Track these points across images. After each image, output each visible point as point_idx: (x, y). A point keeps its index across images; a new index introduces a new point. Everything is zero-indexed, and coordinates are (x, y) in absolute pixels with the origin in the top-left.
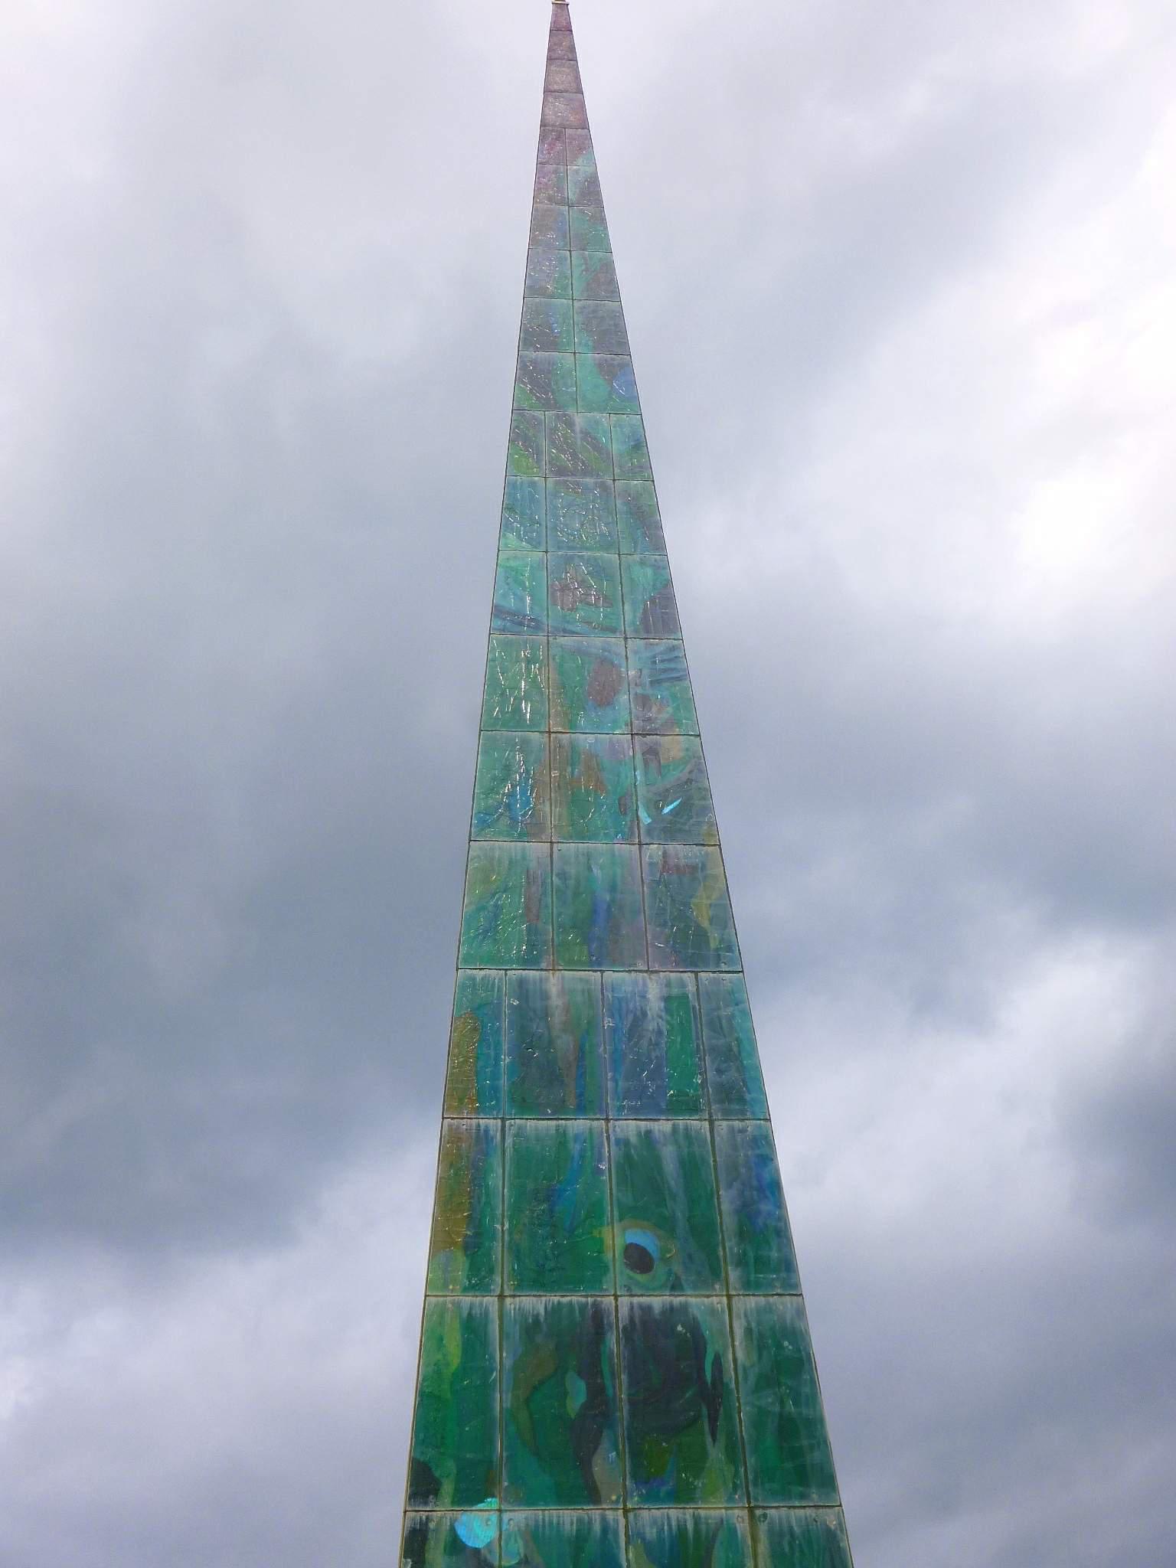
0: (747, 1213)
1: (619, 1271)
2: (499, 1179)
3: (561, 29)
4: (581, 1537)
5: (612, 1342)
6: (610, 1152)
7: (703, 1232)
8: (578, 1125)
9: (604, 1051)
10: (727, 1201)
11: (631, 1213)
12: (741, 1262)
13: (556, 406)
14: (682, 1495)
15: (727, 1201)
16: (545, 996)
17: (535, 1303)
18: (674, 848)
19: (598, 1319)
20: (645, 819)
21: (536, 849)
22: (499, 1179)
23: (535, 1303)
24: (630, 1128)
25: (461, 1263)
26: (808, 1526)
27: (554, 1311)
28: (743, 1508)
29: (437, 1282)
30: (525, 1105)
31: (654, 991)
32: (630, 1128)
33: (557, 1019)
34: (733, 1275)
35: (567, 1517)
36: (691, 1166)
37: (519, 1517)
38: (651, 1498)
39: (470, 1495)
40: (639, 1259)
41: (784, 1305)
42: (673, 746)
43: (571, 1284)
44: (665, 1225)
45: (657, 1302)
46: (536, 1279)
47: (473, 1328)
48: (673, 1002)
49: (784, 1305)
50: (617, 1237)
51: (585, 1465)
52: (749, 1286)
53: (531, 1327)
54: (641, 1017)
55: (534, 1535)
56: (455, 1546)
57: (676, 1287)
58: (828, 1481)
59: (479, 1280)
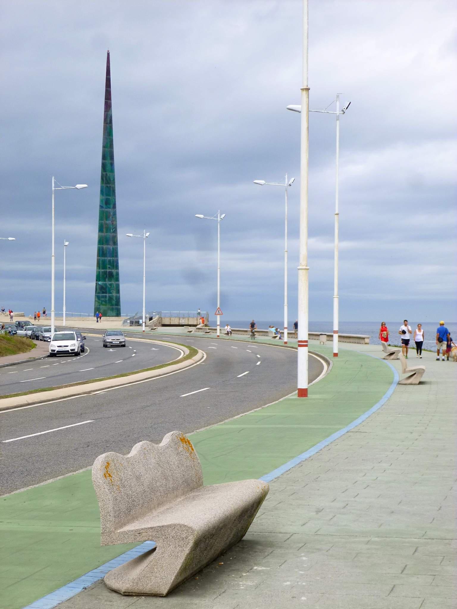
0: (116, 265)
1: (108, 269)
2: (101, 262)
3: (108, 54)
4: (105, 283)
5: (107, 273)
6: (108, 260)
7: (113, 266)
8: (106, 258)
9: (108, 252)
10: (115, 264)
11: (109, 264)
12: (116, 268)
13: (106, 172)
14: (111, 281)
15: (115, 264)
16: (104, 248)
17: (103, 270)
18: (114, 234)
19: (106, 271)
20: (112, 231)
21: (103, 234)
22: (101, 262)
23: (103, 270)
24: (109, 258)
25: (98, 268)
26: (317, 508)
27: (104, 271)
28: (197, 323)
29: (97, 269)
30: (102, 256)
31: (111, 248)
32: (109, 258)
33: (105, 250)
34: (115, 269)
35: (104, 282)
36: (113, 262)
37: (102, 282)
38: (109, 282)
39: (99, 281)
40: (109, 268)
41: (119, 307)
42: (114, 223)
43: (106, 269)
44: (111, 265)
45: (110, 270)
46: (103, 269)
47: (99, 272)
48: (113, 249)
49: (118, 271)
50: (108, 266)
51: (105, 280)
52: (116, 270)
53: (103, 272)
54: (110, 249)
55: (103, 283)
56: (98, 284)
57: (111, 269)
58: (119, 281)
59: (99, 268)
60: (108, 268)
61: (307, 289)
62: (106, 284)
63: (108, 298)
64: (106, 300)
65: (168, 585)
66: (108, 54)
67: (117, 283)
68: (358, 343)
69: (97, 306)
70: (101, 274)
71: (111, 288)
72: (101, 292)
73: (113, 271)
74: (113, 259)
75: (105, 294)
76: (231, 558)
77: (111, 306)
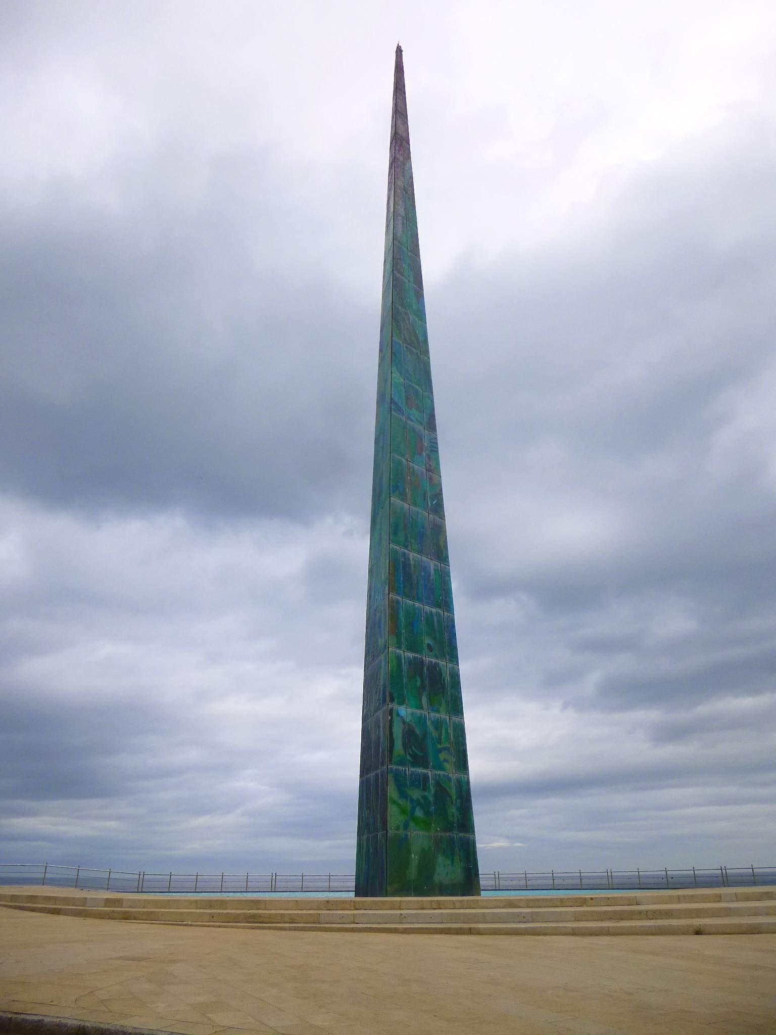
3: (399, 51)
17: (411, 655)
19: (422, 662)
27: (415, 658)
37: (409, 710)
46: (411, 648)
53: (410, 662)
60: (425, 646)
61: (395, 745)
62: (422, 721)
63: (433, 790)
64: (425, 798)
65: (391, 829)
66: (399, 51)
67: (455, 719)
68: (767, 915)
69: (398, 828)
70: (405, 668)
71: (440, 743)
72: (409, 758)
73: (442, 663)
74: (438, 615)
75: (420, 770)
76: (425, 888)
77: (445, 830)
